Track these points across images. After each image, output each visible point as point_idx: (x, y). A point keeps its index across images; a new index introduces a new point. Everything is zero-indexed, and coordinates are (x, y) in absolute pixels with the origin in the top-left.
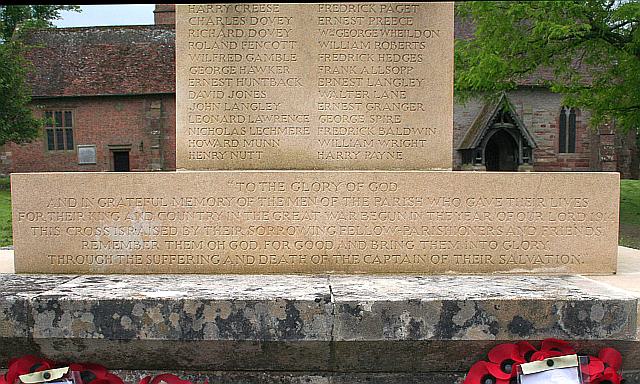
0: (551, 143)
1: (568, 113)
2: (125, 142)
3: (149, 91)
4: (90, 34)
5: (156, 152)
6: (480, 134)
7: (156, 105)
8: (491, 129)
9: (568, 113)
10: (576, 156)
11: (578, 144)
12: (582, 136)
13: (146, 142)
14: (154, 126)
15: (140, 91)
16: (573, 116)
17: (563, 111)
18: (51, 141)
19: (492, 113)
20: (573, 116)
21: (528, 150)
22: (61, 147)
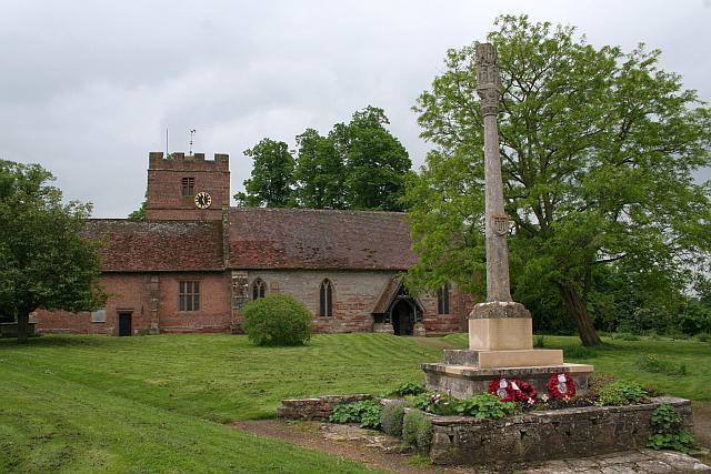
0: (432, 308)
1: (326, 287)
2: (129, 306)
3: (150, 269)
4: (101, 225)
5: (155, 314)
6: (388, 303)
7: (155, 280)
8: (395, 299)
9: (326, 287)
10: (450, 316)
11: (450, 308)
12: (453, 303)
13: (146, 307)
14: (153, 294)
15: (143, 269)
16: (446, 289)
17: (323, 286)
18: (182, 302)
19: (395, 288)
20: (446, 289)
21: (421, 313)
22: (189, 309)
